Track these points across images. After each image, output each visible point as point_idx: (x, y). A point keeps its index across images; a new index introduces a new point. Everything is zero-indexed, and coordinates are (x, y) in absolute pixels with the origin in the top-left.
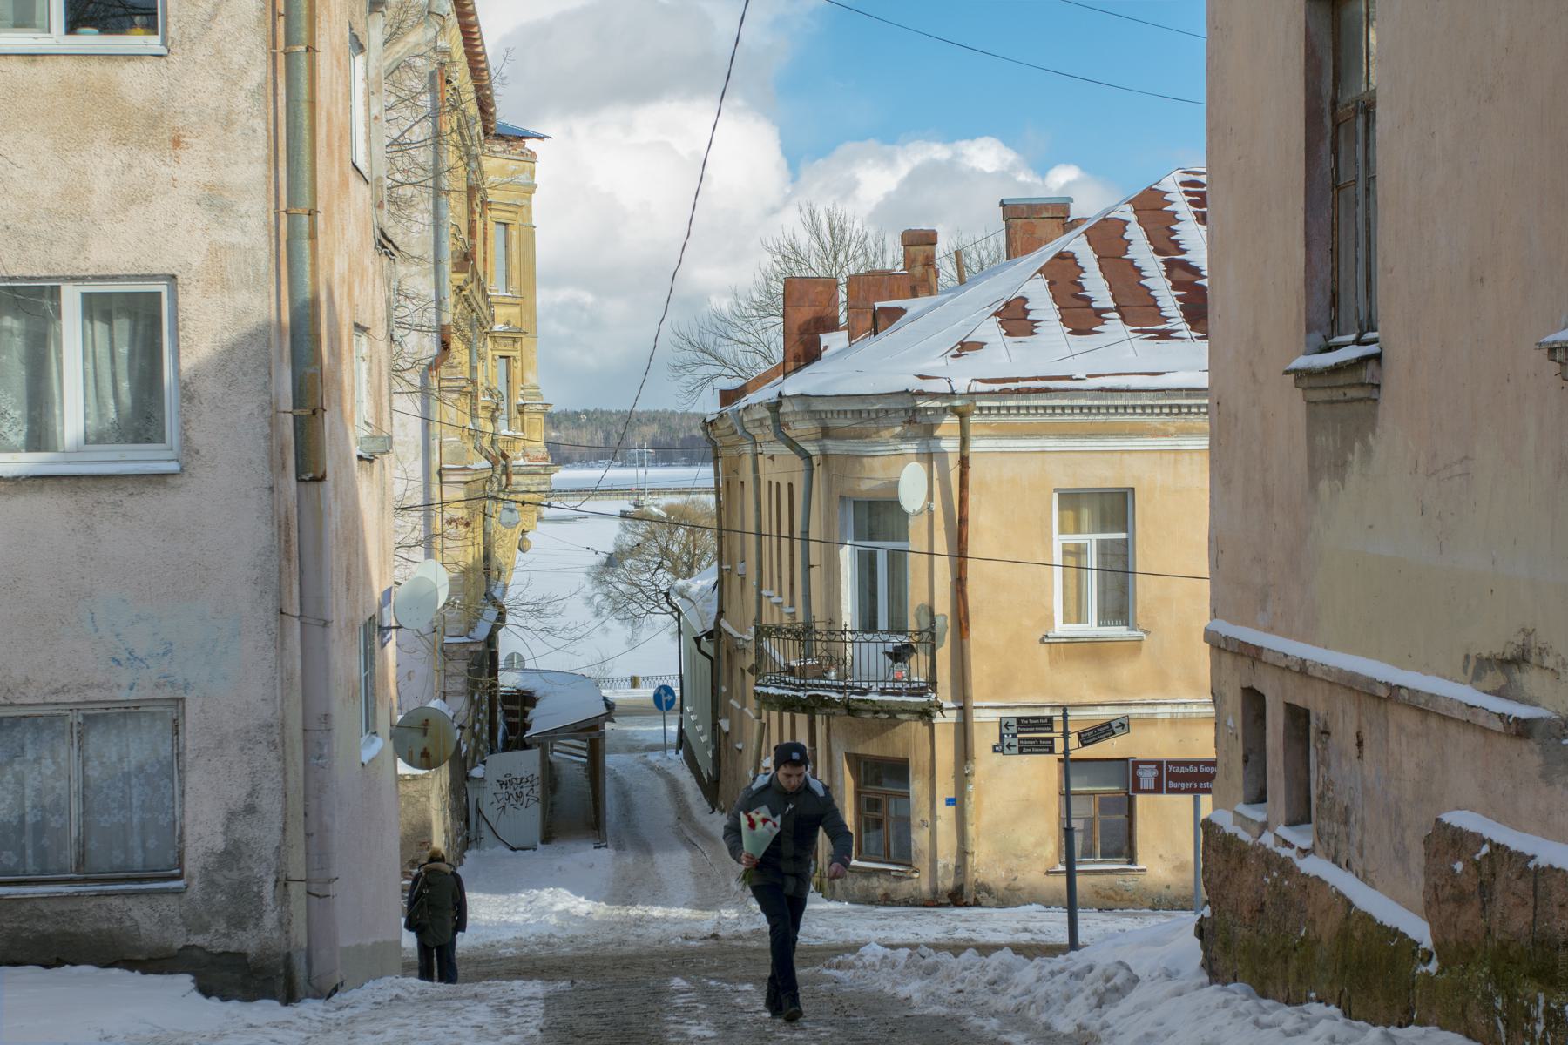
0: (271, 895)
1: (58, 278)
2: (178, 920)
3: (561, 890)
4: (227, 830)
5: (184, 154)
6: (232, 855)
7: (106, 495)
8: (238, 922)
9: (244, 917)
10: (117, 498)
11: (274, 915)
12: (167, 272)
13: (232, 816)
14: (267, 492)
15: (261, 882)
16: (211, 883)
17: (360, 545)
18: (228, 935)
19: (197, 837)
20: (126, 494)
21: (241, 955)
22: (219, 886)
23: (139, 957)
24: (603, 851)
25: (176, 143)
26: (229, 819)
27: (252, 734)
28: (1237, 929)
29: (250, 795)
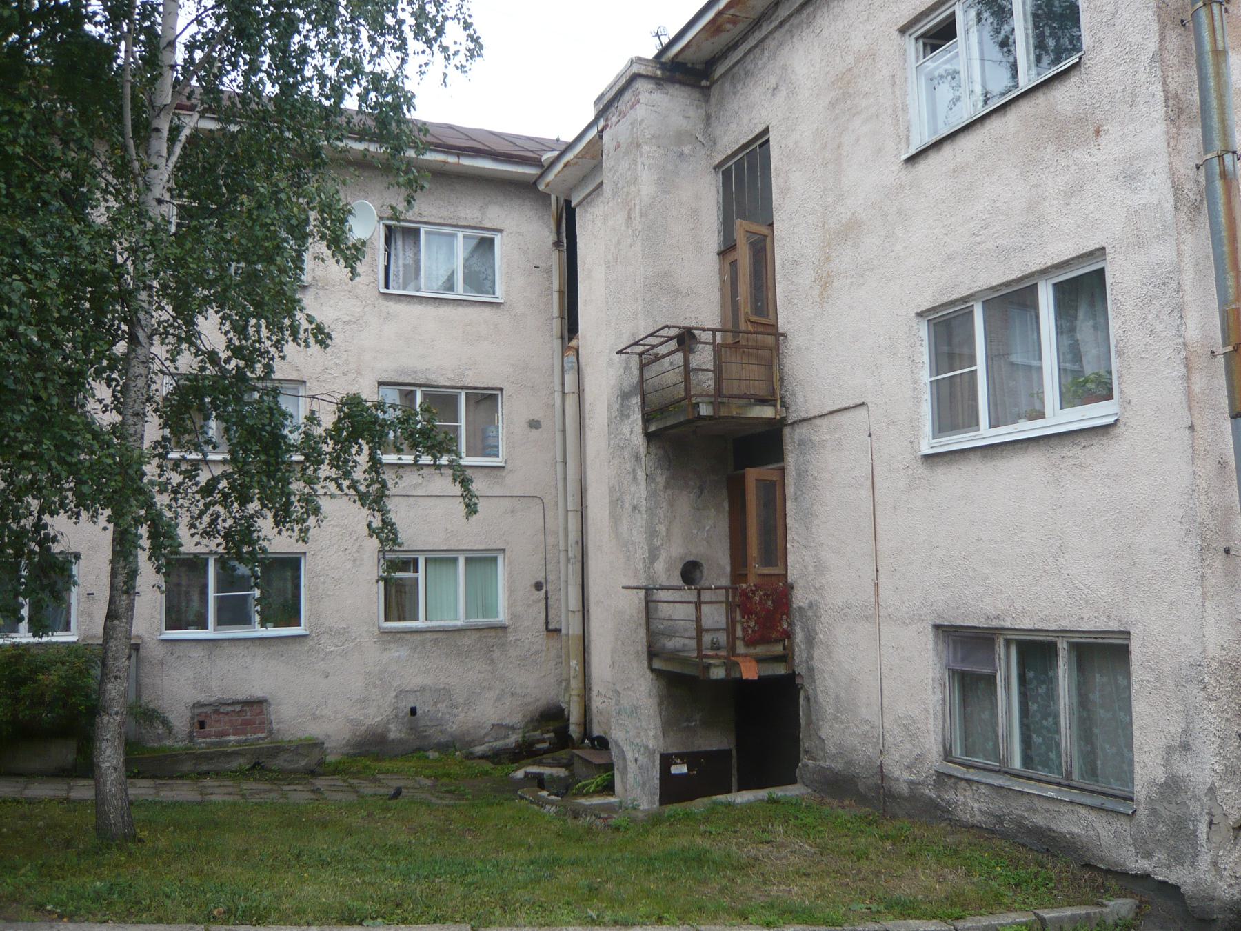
0: (1205, 836)
1: (1032, 275)
2: (1130, 841)
3: (756, 678)
4: (1167, 763)
5: (1103, 140)
6: (1173, 787)
7: (1067, 451)
8: (1178, 858)
9: (1182, 852)
10: (1075, 451)
11: (1208, 858)
12: (1098, 246)
13: (1170, 750)
14: (1187, 432)
15: (1196, 820)
16: (1154, 812)
17: (518, 142)
18: (1168, 867)
19: (1142, 765)
20: (1080, 447)
21: (1176, 888)
22: (1161, 817)
23: (1101, 866)
24: (479, 507)
25: (1097, 133)
26: (1167, 753)
27: (1184, 672)
28: (108, 400)
29: (1185, 732)
